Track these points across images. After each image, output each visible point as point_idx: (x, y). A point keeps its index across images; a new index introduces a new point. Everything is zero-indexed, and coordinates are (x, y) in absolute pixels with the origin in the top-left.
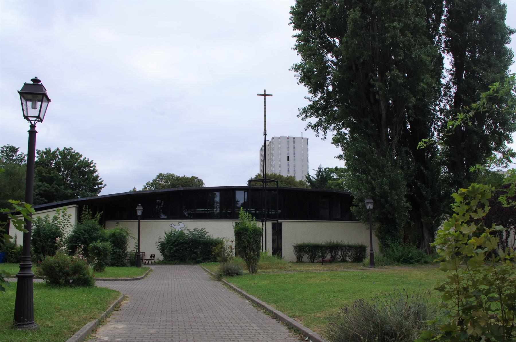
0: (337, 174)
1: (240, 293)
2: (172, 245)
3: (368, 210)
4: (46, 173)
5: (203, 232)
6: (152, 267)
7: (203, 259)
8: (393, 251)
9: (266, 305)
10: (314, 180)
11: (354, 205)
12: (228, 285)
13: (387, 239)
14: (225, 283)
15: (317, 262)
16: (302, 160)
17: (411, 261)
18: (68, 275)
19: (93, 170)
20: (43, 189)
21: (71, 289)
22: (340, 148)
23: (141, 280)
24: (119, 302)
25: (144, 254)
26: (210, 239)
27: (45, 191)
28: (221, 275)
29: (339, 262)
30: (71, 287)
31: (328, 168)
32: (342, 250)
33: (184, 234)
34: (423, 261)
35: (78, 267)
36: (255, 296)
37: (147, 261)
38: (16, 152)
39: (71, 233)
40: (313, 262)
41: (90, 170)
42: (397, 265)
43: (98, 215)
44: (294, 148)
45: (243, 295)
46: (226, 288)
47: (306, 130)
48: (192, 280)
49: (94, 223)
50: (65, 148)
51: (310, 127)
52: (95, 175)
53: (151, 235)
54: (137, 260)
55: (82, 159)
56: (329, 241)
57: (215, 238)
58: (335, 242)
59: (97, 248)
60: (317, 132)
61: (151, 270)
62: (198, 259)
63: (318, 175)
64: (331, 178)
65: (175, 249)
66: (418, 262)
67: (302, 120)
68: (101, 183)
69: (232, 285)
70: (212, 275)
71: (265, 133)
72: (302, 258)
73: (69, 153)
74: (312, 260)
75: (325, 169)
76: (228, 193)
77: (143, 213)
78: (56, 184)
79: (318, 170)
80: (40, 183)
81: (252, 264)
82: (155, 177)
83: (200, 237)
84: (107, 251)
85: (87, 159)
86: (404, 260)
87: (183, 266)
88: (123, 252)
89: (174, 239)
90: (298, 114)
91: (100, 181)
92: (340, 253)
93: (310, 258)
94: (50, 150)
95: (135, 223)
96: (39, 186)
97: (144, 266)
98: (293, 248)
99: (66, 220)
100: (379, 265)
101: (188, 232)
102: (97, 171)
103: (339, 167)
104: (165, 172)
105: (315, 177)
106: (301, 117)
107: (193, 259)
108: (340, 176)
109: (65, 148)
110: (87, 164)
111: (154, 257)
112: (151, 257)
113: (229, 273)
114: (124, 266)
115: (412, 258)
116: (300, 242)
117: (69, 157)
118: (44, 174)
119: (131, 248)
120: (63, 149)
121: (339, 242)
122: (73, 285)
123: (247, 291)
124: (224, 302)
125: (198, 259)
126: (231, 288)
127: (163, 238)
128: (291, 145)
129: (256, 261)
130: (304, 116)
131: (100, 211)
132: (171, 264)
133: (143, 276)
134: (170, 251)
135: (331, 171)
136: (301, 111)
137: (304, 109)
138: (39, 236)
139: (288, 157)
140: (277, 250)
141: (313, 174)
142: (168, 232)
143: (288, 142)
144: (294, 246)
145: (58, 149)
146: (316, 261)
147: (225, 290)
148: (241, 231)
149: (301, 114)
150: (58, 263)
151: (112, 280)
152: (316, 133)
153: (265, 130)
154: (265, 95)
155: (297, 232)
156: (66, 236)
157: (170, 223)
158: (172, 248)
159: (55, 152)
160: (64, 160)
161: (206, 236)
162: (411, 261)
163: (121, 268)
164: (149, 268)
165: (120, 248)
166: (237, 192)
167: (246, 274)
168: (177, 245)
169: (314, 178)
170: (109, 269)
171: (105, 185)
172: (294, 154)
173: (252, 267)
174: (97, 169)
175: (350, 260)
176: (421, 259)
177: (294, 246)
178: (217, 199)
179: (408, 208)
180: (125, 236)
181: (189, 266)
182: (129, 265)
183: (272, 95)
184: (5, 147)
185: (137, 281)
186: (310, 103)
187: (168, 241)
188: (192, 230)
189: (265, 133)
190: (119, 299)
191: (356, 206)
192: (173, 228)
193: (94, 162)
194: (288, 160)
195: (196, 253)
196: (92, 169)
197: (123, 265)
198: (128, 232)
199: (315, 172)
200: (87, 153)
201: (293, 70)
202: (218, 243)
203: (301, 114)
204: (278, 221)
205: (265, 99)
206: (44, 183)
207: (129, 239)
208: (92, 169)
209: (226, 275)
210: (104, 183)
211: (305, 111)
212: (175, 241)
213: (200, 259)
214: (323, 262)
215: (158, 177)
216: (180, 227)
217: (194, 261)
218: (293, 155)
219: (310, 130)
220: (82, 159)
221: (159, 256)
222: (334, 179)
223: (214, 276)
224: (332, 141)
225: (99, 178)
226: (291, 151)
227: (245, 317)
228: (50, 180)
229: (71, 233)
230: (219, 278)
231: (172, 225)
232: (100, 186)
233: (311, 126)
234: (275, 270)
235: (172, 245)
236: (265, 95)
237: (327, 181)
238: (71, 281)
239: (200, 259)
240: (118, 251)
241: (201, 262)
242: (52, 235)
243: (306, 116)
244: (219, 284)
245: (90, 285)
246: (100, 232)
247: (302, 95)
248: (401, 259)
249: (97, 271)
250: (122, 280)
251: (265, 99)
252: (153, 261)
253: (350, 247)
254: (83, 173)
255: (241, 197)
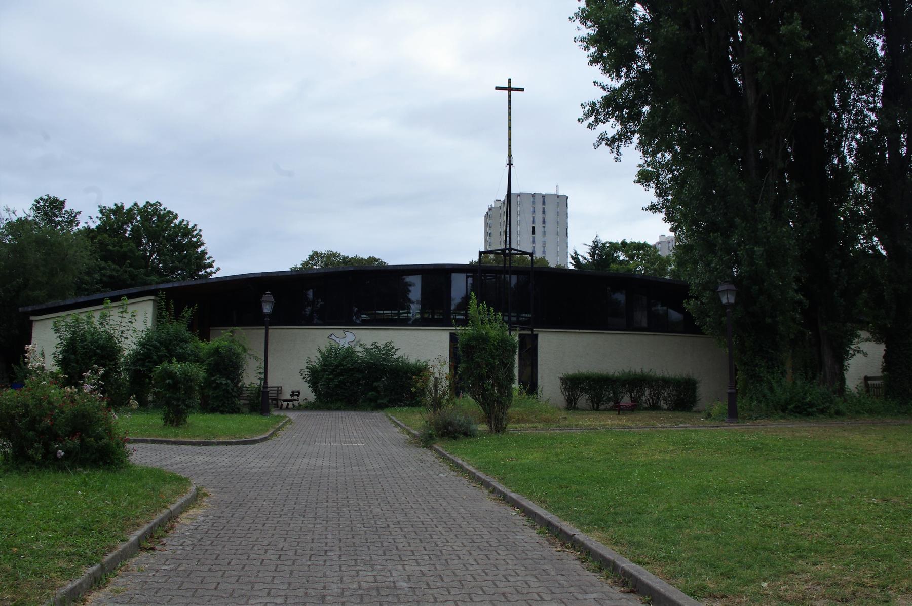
0: (626, 253)
1: (487, 485)
2: (331, 373)
3: (724, 307)
4: (114, 246)
5: (388, 349)
6: (292, 415)
7: (389, 402)
8: (771, 389)
9: (581, 536)
10: (584, 262)
11: (692, 297)
12: (449, 459)
13: (757, 365)
14: (441, 455)
15: (606, 410)
16: (557, 234)
17: (810, 410)
18: (56, 437)
19: (197, 242)
20: (109, 273)
21: (61, 477)
22: (652, 191)
23: (261, 445)
24: (173, 517)
25: (279, 390)
26: (403, 362)
27: (111, 277)
28: (431, 436)
29: (646, 409)
30: (63, 469)
31: (610, 243)
32: (651, 387)
33: (353, 352)
34: (833, 411)
35: (84, 416)
36: (530, 497)
37: (285, 404)
38: (61, 209)
39: (134, 347)
40: (597, 409)
41: (191, 241)
42: (782, 417)
43: (187, 313)
44: (544, 212)
45: (494, 491)
46: (448, 468)
47: (596, 147)
48: (371, 440)
49: (180, 328)
50: (148, 202)
51: (604, 142)
52: (199, 250)
53: (291, 356)
54: (264, 402)
55: (177, 222)
56: (627, 371)
57: (412, 361)
58: (639, 371)
59: (171, 375)
60: (618, 153)
61: (290, 420)
62: (380, 401)
63: (592, 255)
64: (615, 260)
65: (336, 382)
66: (822, 411)
67: (588, 127)
68: (210, 266)
69: (460, 461)
70: (409, 433)
71: (510, 161)
72: (575, 400)
73: (156, 212)
74: (596, 405)
75: (604, 244)
76: (437, 276)
77: (274, 310)
78: (131, 265)
79: (592, 244)
80: (103, 264)
81: (496, 414)
82: (306, 258)
83: (384, 360)
84: (191, 380)
85: (185, 223)
86: (796, 407)
87: (352, 413)
88: (236, 385)
89: (336, 363)
90: (581, 116)
91: (208, 261)
92: (647, 392)
93: (592, 402)
94: (122, 207)
95: (260, 332)
96: (101, 269)
97: (276, 414)
98: (559, 383)
99: (131, 324)
100: (744, 418)
101: (361, 350)
102: (203, 244)
103: (628, 241)
104: (323, 249)
105: (588, 257)
106: (586, 123)
107: (371, 400)
108: (631, 257)
109: (148, 202)
110: (186, 231)
111: (298, 395)
112: (292, 396)
113: (448, 432)
114: (236, 412)
115: (811, 405)
116: (571, 371)
117: (155, 219)
118: (110, 248)
119: (250, 378)
120: (144, 203)
121: (646, 370)
122: (66, 463)
123: (502, 480)
124: (454, 514)
125: (380, 401)
126: (458, 468)
127: (315, 359)
128: (539, 207)
129: (504, 407)
130: (592, 119)
131: (191, 305)
132: (329, 409)
133: (267, 434)
134: (328, 384)
135: (614, 247)
136: (587, 109)
137: (593, 105)
138: (75, 352)
139: (533, 228)
140: (531, 385)
141: (584, 253)
142: (324, 350)
143: (533, 202)
144: (561, 379)
145: (136, 204)
146: (602, 407)
147: (445, 473)
148: (474, 343)
149: (587, 116)
150: (26, 406)
151: (198, 444)
152: (614, 154)
153: (510, 156)
154: (510, 89)
155: (563, 353)
156: (126, 352)
157: (331, 332)
158: (332, 380)
159: (131, 209)
160: (147, 224)
161: (395, 357)
162: (810, 410)
163: (228, 416)
164: (286, 417)
165: (228, 378)
166: (454, 275)
167: (482, 434)
168: (341, 374)
169: (585, 259)
170: (198, 420)
171: (218, 269)
172: (544, 222)
173: (496, 418)
174: (203, 239)
175: (665, 407)
176: (829, 408)
177: (561, 379)
178: (415, 293)
179: (800, 303)
180: (239, 354)
181: (364, 413)
182: (245, 410)
183: (522, 90)
184: (41, 199)
185: (252, 446)
186: (605, 93)
187: (325, 365)
188: (369, 346)
189: (510, 161)
190: (172, 507)
191: (696, 298)
192: (333, 342)
193: (198, 227)
194: (533, 233)
195: (375, 389)
196: (195, 239)
197: (235, 410)
198: (246, 346)
199: (588, 249)
200: (185, 210)
201: (577, 21)
202: (419, 371)
203: (587, 116)
204: (532, 331)
205: (510, 96)
206: (110, 263)
207: (247, 359)
208: (195, 239)
209: (443, 436)
210: (216, 265)
211: (593, 110)
212: (337, 366)
213: (385, 401)
214: (618, 409)
215: (311, 258)
216: (347, 339)
217: (372, 404)
218: (541, 225)
219: (604, 148)
220: (177, 222)
221: (308, 394)
222: (622, 262)
223: (415, 436)
224: (637, 179)
225: (207, 256)
226: (539, 217)
227: (534, 583)
228: (121, 258)
229: (134, 347)
230: (426, 441)
231: (333, 337)
232: (208, 270)
233: (607, 139)
234: (537, 425)
235: (331, 373)
236: (510, 89)
237: (609, 264)
238: (61, 453)
239: (385, 401)
240: (224, 382)
241: (387, 407)
242: (98, 351)
243: (597, 121)
244: (429, 456)
245: (112, 463)
246: (190, 346)
247: (592, 81)
248: (790, 407)
249: (172, 422)
250: (219, 444)
251: (510, 96)
252: (296, 403)
253: (666, 382)
254: (179, 247)
255: (459, 286)
